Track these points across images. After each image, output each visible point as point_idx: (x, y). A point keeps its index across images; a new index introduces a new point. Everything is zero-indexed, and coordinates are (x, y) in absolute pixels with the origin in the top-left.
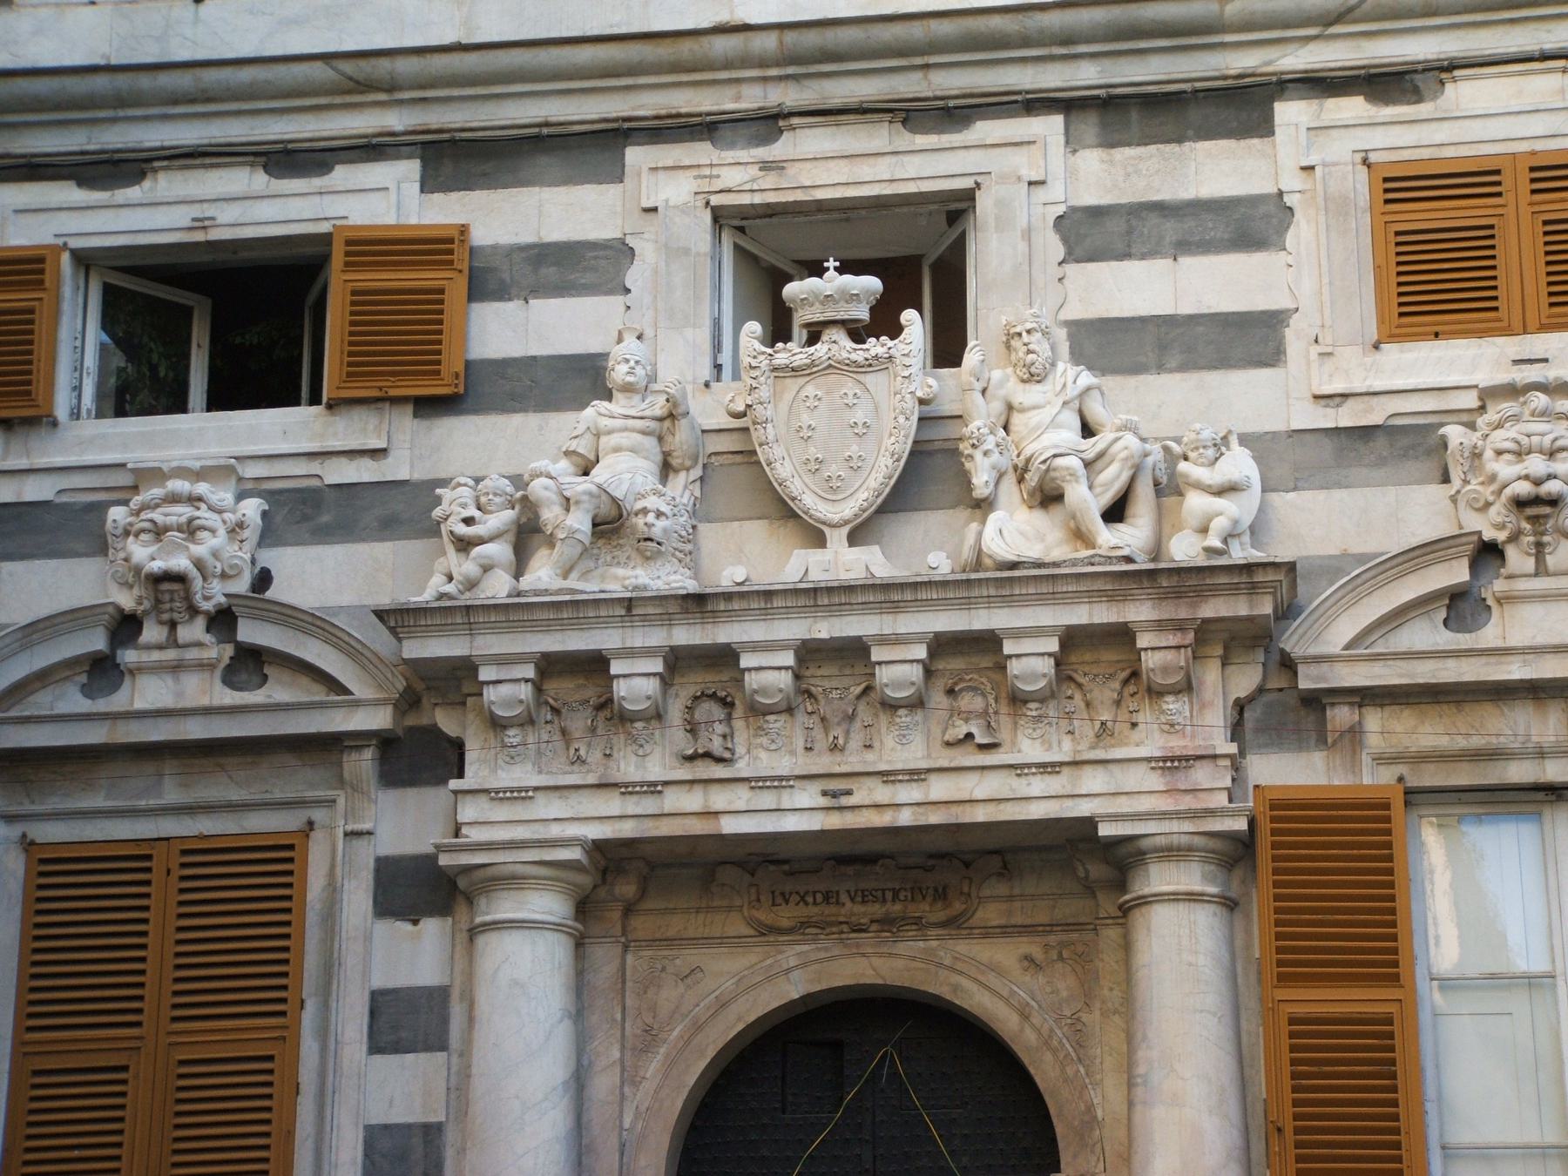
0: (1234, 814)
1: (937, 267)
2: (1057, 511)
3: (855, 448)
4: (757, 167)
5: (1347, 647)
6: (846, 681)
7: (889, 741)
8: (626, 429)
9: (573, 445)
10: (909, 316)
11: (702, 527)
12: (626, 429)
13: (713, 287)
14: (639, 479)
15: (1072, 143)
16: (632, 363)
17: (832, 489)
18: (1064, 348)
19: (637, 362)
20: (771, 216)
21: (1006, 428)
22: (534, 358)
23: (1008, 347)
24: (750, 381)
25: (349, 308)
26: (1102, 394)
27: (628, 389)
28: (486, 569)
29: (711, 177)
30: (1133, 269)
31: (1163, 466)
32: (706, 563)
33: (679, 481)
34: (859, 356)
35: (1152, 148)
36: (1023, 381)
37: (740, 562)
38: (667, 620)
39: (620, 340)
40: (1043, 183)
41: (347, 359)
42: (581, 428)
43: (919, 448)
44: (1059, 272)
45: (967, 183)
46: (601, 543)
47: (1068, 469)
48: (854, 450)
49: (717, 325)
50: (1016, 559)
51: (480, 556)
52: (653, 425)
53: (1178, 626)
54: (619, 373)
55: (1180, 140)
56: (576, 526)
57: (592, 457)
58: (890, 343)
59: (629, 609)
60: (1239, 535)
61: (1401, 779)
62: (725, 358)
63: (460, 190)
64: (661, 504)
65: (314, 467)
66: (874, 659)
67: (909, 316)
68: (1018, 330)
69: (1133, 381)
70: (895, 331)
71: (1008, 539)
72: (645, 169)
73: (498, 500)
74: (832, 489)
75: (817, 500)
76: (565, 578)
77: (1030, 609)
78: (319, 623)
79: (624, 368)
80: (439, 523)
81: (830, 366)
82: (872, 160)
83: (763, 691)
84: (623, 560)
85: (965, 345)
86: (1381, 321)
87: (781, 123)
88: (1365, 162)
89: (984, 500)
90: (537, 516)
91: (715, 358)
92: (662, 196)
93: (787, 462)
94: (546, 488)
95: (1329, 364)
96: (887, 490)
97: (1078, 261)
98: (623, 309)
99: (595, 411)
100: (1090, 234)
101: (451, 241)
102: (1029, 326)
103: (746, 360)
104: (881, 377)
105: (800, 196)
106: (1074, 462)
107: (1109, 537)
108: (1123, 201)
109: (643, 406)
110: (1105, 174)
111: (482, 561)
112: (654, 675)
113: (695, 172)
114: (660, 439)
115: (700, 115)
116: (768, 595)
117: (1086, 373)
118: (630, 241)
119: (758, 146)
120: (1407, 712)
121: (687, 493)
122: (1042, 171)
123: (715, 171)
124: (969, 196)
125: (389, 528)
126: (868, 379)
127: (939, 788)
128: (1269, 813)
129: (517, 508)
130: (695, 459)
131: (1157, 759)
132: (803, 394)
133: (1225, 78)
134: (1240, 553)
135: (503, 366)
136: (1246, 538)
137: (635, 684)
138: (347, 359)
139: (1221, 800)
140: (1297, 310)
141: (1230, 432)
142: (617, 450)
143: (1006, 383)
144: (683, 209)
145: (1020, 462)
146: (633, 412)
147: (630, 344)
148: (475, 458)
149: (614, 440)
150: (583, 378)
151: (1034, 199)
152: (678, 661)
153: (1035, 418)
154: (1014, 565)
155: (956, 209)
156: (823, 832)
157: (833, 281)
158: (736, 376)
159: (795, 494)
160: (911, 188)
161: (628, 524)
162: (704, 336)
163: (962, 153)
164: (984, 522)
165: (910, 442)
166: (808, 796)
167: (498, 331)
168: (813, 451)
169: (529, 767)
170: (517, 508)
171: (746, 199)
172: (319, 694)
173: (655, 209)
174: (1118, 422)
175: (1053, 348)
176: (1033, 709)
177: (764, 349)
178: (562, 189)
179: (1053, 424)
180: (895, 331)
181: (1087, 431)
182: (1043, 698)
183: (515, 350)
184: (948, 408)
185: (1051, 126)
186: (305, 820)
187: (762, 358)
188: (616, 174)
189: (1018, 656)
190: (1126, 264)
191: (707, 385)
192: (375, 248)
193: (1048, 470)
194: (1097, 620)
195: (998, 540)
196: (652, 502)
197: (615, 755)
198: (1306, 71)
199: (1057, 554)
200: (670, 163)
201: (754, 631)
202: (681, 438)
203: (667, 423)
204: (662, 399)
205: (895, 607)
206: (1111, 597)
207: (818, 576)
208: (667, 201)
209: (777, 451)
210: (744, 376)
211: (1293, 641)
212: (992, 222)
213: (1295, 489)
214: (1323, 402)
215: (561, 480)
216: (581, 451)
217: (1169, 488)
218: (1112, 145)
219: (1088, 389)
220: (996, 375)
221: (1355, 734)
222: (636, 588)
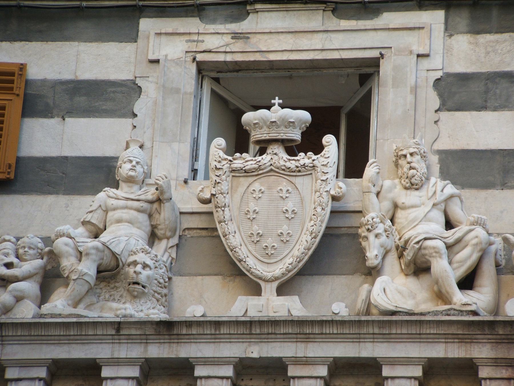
1: (350, 115)
2: (425, 279)
3: (285, 227)
4: (230, 36)
8: (126, 207)
9: (89, 217)
10: (329, 139)
11: (175, 279)
12: (126, 207)
13: (194, 116)
14: (133, 241)
16: (134, 163)
17: (268, 255)
18: (436, 168)
19: (138, 163)
20: (238, 71)
21: (392, 220)
22: (66, 158)
23: (397, 165)
24: (215, 178)
26: (462, 201)
27: (130, 180)
28: (19, 299)
29: (198, 41)
30: (488, 117)
31: (502, 253)
32: (176, 304)
33: (161, 246)
34: (292, 165)
35: (506, 36)
36: (406, 188)
37: (200, 303)
38: (145, 340)
39: (127, 147)
40: (427, 56)
42: (95, 206)
43: (331, 232)
44: (436, 117)
45: (375, 54)
46: (102, 285)
47: (434, 248)
48: (285, 228)
49: (196, 143)
50: (394, 309)
51: (15, 290)
52: (145, 205)
54: (125, 169)
56: (85, 271)
57: (101, 226)
58: (314, 157)
59: (118, 330)
62: (200, 165)
63: (21, 40)
64: (148, 260)
66: (290, 374)
67: (329, 139)
68: (404, 152)
69: (483, 194)
70: (318, 149)
71: (390, 296)
72: (152, 33)
73: (31, 252)
74: (268, 255)
75: (257, 262)
76: (75, 305)
77: (402, 344)
79: (128, 166)
81: (272, 170)
82: (309, 35)
84: (117, 298)
85: (367, 161)
87: (248, 7)
89: (374, 268)
90: (59, 264)
91: (193, 165)
92: (163, 52)
93: (237, 235)
96: (306, 258)
97: (449, 110)
98: (131, 127)
99: (105, 196)
100: (458, 92)
101: (13, 74)
102: (412, 150)
103: (213, 164)
104: (307, 180)
105: (258, 57)
106: (439, 244)
107: (460, 297)
108: (483, 70)
109: (140, 192)
111: (16, 294)
112: (133, 378)
113: (187, 38)
114: (150, 216)
116: (217, 324)
117: (450, 186)
118: (139, 82)
119: (231, 22)
121: (167, 255)
122: (427, 47)
123: (201, 38)
124: (374, 64)
126: (298, 181)
129: (45, 258)
130: (174, 231)
132: (251, 189)
142: (119, 221)
143: (394, 189)
144: (177, 62)
145: (401, 243)
146: (132, 196)
147: (134, 150)
150: (100, 172)
151: (420, 67)
153: (413, 213)
154: (393, 313)
155: (365, 72)
157: (277, 113)
158: (207, 177)
159: (242, 257)
160: (336, 55)
161: (122, 272)
162: (186, 148)
163: (372, 34)
164: (373, 284)
165: (324, 225)
167: (43, 138)
168: (256, 228)
170: (45, 258)
171: (221, 58)
173: (157, 61)
174: (472, 219)
175: (428, 168)
177: (226, 157)
178: (94, 44)
179: (426, 218)
180: (318, 149)
181: (449, 225)
183: (53, 152)
184: (352, 206)
187: (224, 162)
188: (133, 37)
189: (393, 378)
190: (482, 113)
191: (186, 182)
193: (420, 249)
194: (450, 355)
195: (382, 294)
196: (141, 257)
199: (424, 307)
200: (170, 30)
202: (165, 216)
203: (156, 205)
204: (153, 190)
205: (307, 338)
206: (462, 339)
207: (253, 314)
208: (166, 56)
209: (231, 227)
210: (212, 175)
212: (390, 82)
215: (77, 239)
216: (93, 221)
218: (479, 32)
219: (452, 197)
220: (387, 183)
222: (125, 316)
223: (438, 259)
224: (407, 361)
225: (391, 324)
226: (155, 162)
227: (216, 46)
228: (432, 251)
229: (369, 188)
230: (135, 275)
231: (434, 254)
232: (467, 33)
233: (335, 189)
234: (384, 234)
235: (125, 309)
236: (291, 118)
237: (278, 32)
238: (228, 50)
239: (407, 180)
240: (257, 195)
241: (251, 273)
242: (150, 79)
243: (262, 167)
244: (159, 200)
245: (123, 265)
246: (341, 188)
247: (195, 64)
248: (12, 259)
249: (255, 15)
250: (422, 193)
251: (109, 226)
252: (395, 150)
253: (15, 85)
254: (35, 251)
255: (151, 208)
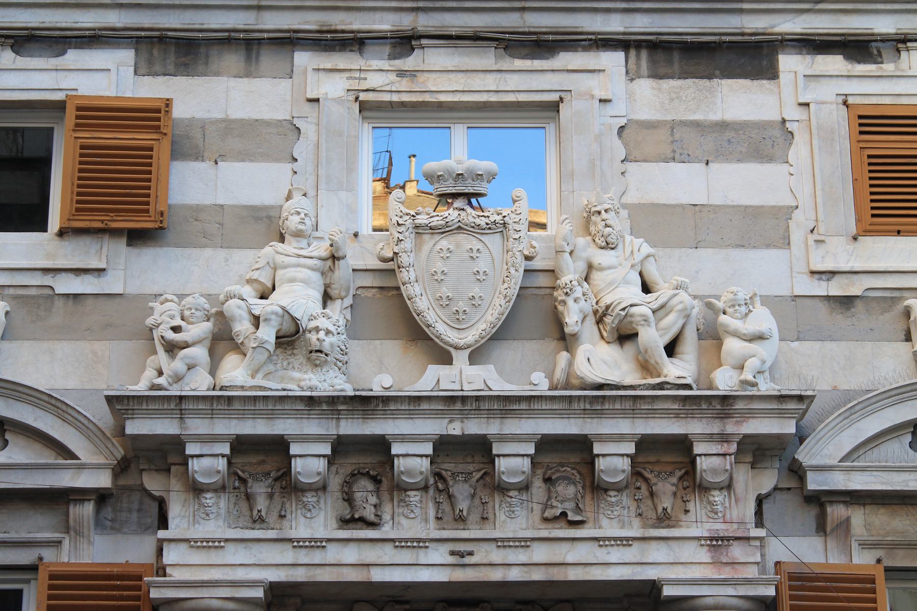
0: (767, 582)
2: (629, 347)
3: (477, 289)
5: (840, 462)
6: (471, 468)
7: (501, 516)
8: (298, 266)
9: (255, 275)
15: (631, 76)
16: (302, 215)
19: (306, 215)
25: (78, 159)
27: (298, 234)
29: (360, 79)
35: (690, 82)
36: (602, 248)
39: (289, 197)
40: (610, 101)
41: (76, 198)
45: (554, 97)
46: (279, 351)
47: (642, 316)
48: (476, 291)
50: (603, 382)
51: (186, 357)
53: (724, 438)
55: (710, 77)
56: (266, 338)
60: (763, 372)
61: (879, 561)
64: (328, 324)
65: (47, 280)
72: (310, 69)
73: (198, 314)
74: (458, 320)
75: (446, 327)
76: (253, 377)
78: (53, 402)
80: (151, 330)
83: (409, 473)
84: (296, 365)
86: (858, 221)
87: (413, 43)
88: (845, 103)
94: (239, 307)
95: (823, 247)
98: (291, 173)
101: (159, 111)
102: (606, 206)
110: (653, 98)
111: (188, 361)
113: (347, 75)
115: (352, 32)
120: (882, 510)
125: (107, 331)
127: (540, 553)
128: (788, 583)
129: (212, 320)
130: (348, 291)
131: (706, 539)
132: (438, 247)
133: (743, 34)
134: (765, 387)
135: (197, 211)
136: (767, 374)
137: (309, 463)
138: (76, 198)
139: (752, 572)
140: (797, 207)
141: (755, 294)
142: (292, 280)
144: (338, 101)
148: (174, 282)
149: (290, 273)
150: (268, 225)
152: (342, 447)
156: (450, 582)
159: (430, 322)
165: (518, 288)
166: (439, 555)
168: (445, 291)
169: (221, 523)
172: (47, 457)
173: (317, 100)
176: (613, 497)
182: (619, 488)
183: (208, 200)
185: (613, 60)
186: (37, 556)
187: (407, 217)
189: (604, 455)
192: (95, 114)
196: (322, 323)
197: (289, 516)
198: (802, 34)
200: (329, 66)
201: (197, 426)
211: (805, 455)
213: (798, 339)
214: (817, 276)
217: (712, 336)
219: (648, 256)
221: (845, 525)
222: (311, 389)
223: (647, 328)
224: (620, 438)
225: (600, 398)
226: (322, 213)
227: (381, 84)
228: (639, 319)
229: (562, 246)
230: (318, 343)
231: (643, 322)
232: (649, 77)
233: (528, 249)
234: (582, 298)
235: (310, 380)
236: (480, 170)
237: (448, 71)
238: (394, 89)
239: (602, 239)
240: (445, 254)
241: (442, 340)
242: (309, 120)
243: (450, 224)
244: (334, 258)
245: (304, 332)
246: (535, 248)
247: (358, 104)
248: (178, 322)
249: (421, 51)
250: (619, 251)
251: (280, 286)
252: (587, 205)
253: (161, 123)
254: (202, 313)
255: (324, 266)
